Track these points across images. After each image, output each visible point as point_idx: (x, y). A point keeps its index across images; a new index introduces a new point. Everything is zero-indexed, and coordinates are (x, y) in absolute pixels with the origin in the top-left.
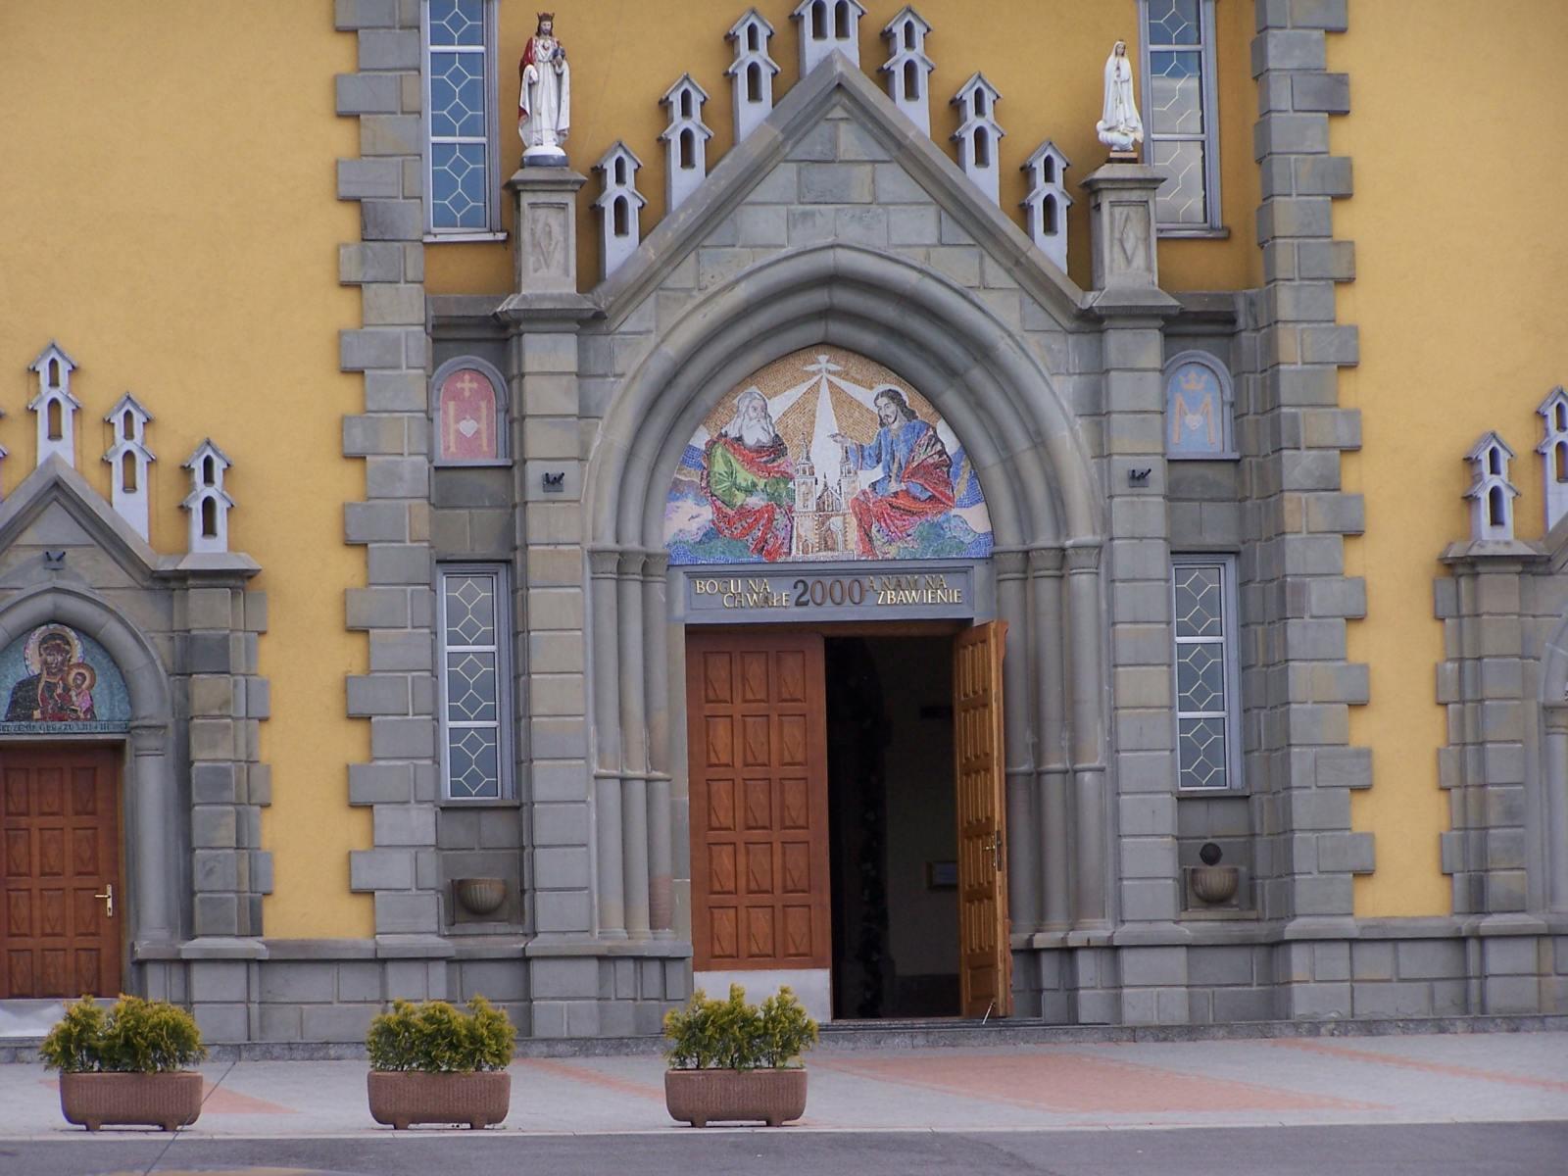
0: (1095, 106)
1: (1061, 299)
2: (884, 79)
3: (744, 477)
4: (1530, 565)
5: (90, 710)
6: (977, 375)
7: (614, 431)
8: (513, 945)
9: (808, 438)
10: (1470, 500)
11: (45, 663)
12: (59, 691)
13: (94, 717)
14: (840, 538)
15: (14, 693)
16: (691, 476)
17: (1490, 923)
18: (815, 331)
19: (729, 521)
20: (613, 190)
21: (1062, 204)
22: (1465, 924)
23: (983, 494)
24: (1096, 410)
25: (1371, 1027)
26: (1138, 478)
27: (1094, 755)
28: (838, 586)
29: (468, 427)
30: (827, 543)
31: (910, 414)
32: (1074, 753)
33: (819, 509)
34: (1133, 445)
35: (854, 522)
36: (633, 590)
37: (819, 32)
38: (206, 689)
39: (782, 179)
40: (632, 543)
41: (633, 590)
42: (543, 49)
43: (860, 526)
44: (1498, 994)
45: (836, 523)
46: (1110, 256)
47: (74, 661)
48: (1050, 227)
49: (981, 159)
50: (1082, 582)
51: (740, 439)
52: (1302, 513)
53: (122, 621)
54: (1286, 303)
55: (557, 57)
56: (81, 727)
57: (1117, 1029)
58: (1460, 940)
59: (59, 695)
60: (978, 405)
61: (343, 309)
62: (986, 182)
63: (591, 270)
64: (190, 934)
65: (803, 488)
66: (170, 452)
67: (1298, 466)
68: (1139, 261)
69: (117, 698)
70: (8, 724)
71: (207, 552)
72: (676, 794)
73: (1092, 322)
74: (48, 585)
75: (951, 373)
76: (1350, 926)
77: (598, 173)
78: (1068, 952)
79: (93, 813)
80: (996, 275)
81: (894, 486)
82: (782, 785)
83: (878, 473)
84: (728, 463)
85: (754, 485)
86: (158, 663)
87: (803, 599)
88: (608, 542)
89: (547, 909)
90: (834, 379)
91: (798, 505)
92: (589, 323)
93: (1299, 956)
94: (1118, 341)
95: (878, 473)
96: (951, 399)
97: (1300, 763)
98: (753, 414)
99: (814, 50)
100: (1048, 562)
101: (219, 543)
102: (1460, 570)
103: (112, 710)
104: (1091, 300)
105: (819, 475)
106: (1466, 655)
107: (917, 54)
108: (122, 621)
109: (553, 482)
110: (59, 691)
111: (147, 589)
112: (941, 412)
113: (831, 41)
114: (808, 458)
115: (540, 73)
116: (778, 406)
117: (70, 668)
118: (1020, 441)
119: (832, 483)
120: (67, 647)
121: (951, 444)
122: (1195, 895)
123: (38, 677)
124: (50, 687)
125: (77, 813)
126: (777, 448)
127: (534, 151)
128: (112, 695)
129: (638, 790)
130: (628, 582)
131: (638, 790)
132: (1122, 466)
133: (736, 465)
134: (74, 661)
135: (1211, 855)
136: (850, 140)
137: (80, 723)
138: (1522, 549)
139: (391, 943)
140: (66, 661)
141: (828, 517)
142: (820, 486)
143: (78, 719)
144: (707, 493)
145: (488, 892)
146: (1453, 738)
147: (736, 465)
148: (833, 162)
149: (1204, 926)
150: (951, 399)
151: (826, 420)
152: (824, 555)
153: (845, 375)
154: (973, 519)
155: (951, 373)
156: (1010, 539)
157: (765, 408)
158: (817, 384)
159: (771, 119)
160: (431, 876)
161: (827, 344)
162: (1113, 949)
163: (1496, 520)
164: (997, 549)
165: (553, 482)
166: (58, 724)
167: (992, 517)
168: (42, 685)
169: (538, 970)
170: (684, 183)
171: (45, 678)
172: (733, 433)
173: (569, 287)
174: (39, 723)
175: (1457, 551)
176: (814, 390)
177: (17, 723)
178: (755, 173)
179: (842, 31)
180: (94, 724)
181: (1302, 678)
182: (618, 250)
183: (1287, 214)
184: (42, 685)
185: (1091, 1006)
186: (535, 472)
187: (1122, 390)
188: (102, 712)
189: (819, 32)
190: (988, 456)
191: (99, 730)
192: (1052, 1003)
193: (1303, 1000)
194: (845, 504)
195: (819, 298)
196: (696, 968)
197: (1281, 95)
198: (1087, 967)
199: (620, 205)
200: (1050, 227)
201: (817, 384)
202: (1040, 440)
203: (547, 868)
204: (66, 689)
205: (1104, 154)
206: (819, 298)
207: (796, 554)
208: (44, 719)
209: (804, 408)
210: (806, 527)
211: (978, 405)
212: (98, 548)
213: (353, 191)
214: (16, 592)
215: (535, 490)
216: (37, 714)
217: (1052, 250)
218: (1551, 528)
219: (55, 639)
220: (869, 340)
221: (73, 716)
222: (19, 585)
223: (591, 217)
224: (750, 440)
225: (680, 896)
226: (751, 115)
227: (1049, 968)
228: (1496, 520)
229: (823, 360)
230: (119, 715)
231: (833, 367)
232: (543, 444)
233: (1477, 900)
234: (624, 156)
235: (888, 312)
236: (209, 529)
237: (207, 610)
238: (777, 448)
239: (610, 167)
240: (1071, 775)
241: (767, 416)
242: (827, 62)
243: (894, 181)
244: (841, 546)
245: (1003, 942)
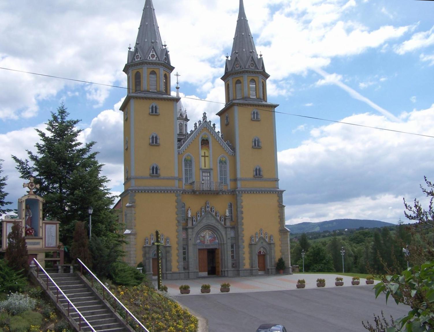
0: (226, 213)
1: (224, 226)
2: (212, 211)
3: (202, 238)
4: (255, 244)
7: (194, 236)
8: (188, 271)
9: (206, 235)
10: (251, 240)
16: (198, 238)
17: (253, 269)
18: (207, 229)
19: (201, 241)
20: (194, 219)
21: (223, 220)
22: (251, 269)
23: (218, 239)
24: (226, 234)
25: (246, 276)
26: (229, 239)
27: (226, 258)
29: (184, 235)
30: (207, 243)
31: (213, 234)
32: (224, 257)
34: (229, 236)
36: (195, 247)
37: (207, 208)
38: (168, 254)
39: (205, 218)
40: (195, 243)
41: (195, 247)
42: (189, 209)
44: (254, 274)
45: (208, 241)
46: (227, 223)
48: (223, 221)
49: (214, 212)
50: (225, 246)
52: (240, 241)
54: (239, 226)
55: (190, 210)
57: (228, 276)
58: (251, 270)
60: (218, 233)
61: (177, 228)
62: (218, 218)
63: (193, 224)
64: (167, 271)
66: (165, 238)
67: (240, 238)
68: (229, 223)
71: (168, 245)
72: (198, 261)
73: (226, 228)
75: (216, 231)
76: (244, 269)
77: (193, 218)
78: (224, 271)
80: (219, 225)
81: (212, 239)
83: (211, 238)
88: (194, 243)
89: (190, 269)
92: (192, 228)
93: (240, 271)
94: (227, 229)
95: (211, 238)
96: (216, 233)
97: (240, 258)
99: (207, 209)
101: (169, 244)
104: (225, 226)
106: (203, 158)
107: (214, 209)
109: (190, 239)
112: (215, 234)
113: (208, 209)
115: (189, 211)
116: (204, 233)
118: (221, 236)
121: (216, 236)
122: (233, 267)
127: (189, 216)
129: (196, 260)
131: (196, 260)
132: (228, 238)
135: (233, 264)
136: (210, 215)
138: (255, 243)
139: (181, 272)
144: (200, 240)
145: (186, 268)
149: (233, 269)
150: (216, 233)
151: (207, 234)
154: (217, 241)
155: (216, 231)
156: (220, 242)
158: (208, 232)
159: (205, 214)
160: (183, 267)
161: (207, 229)
162: (227, 271)
163: (253, 241)
165: (190, 239)
167: (218, 241)
169: (229, 272)
170: (198, 218)
173: (191, 226)
175: (250, 243)
176: (206, 232)
178: (204, 218)
179: (209, 208)
181: (240, 252)
182: (194, 223)
183: (239, 220)
185: (226, 275)
186: (189, 239)
187: (228, 233)
189: (207, 208)
190: (218, 237)
192: (223, 275)
193: (241, 274)
195: (207, 226)
196: (153, 275)
197: (239, 212)
198: (226, 272)
199: (194, 220)
200: (223, 221)
202: (222, 236)
203: (190, 266)
205: (226, 216)
206: (207, 226)
209: (206, 234)
210: (206, 242)
211: (218, 233)
215: (189, 240)
217: (223, 223)
220: (210, 229)
223: (192, 221)
225: (198, 268)
226: (203, 214)
227: (223, 272)
228: (253, 241)
229: (207, 230)
230: (132, 242)
232: (190, 237)
233: (252, 267)
235: (212, 227)
236: (168, 243)
237: (168, 249)
238: (204, 236)
239: (194, 217)
240: (224, 259)
242: (208, 210)
243: (213, 218)
245: (220, 270)
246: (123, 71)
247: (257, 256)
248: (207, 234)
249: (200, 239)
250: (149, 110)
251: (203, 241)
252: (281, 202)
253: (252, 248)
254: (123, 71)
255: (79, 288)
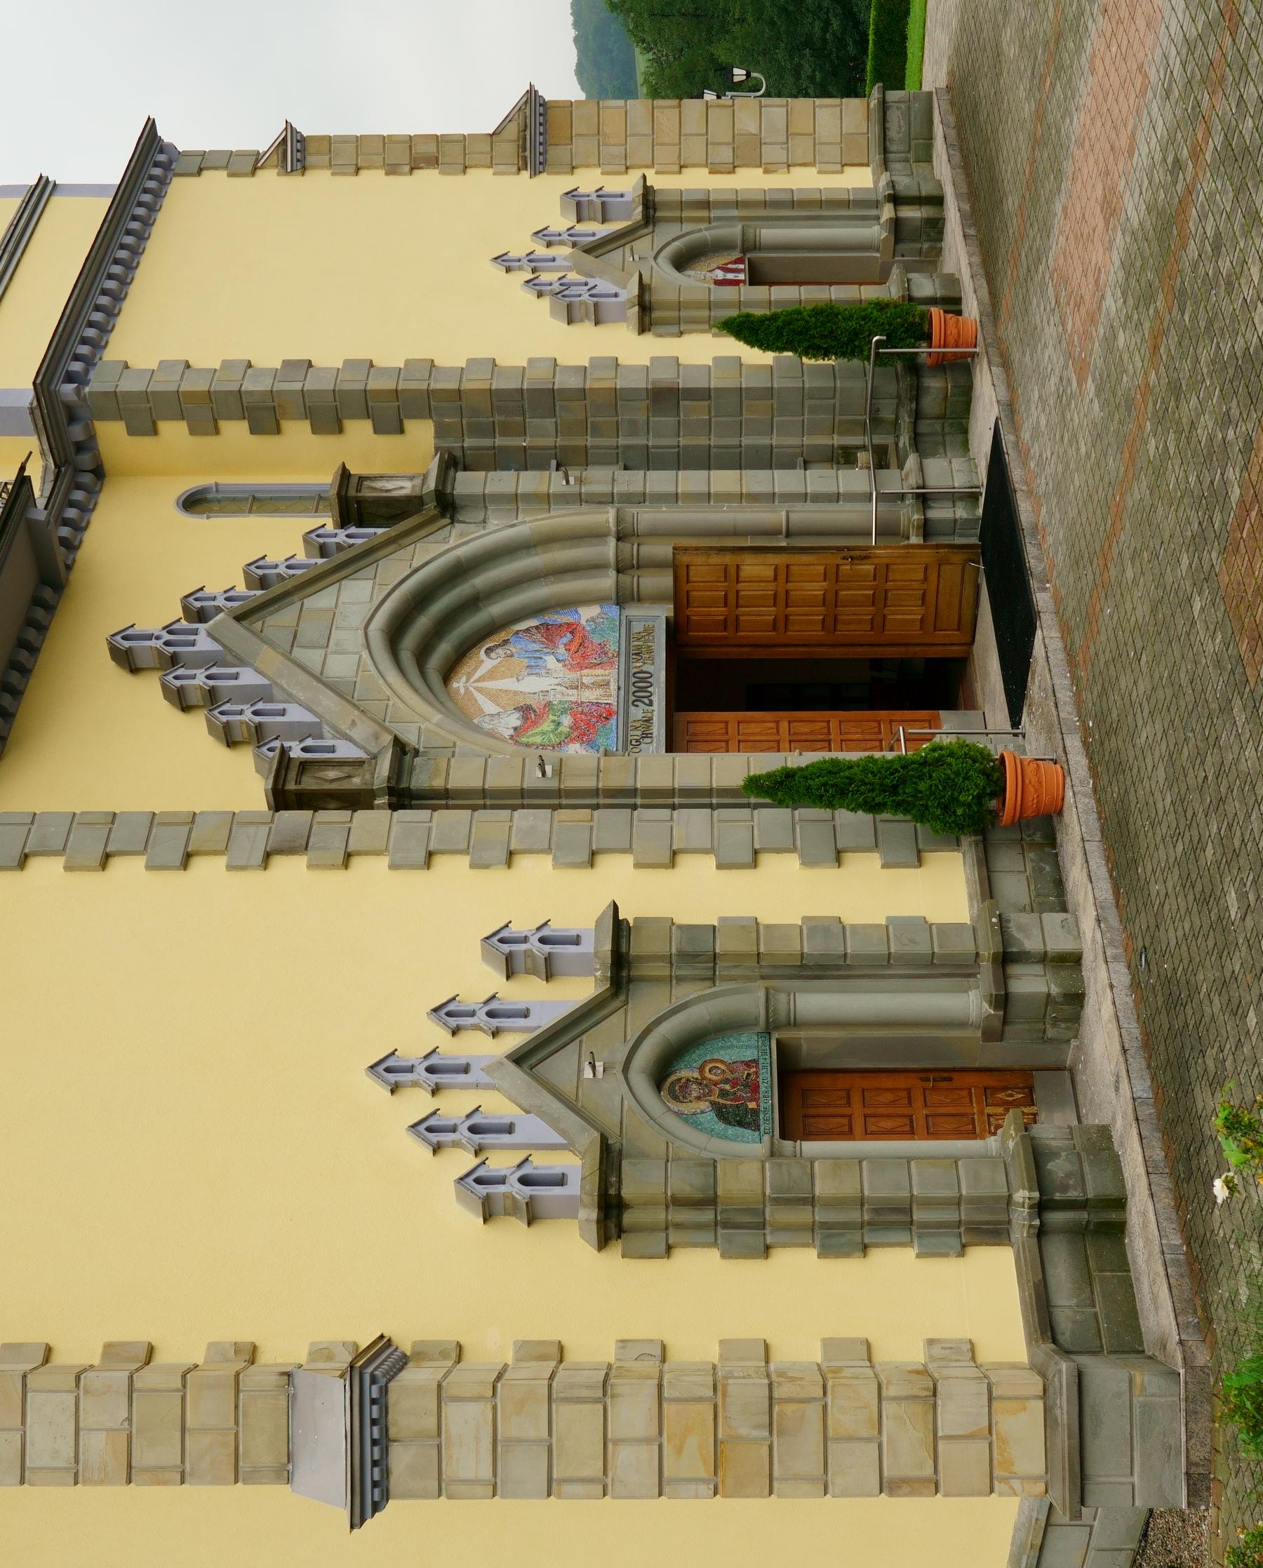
3: (547, 726)
5: (748, 1064)
6: (481, 581)
11: (699, 1098)
12: (728, 1087)
13: (755, 1061)
14: (601, 678)
15: (730, 1124)
28: (636, 694)
33: (577, 688)
35: (585, 672)
43: (591, 668)
47: (696, 1075)
51: (515, 729)
53: (658, 1022)
56: (764, 1071)
59: (733, 1087)
65: (559, 696)
69: (735, 1042)
70: (762, 1128)
74: (621, 1077)
79: (848, 1091)
81: (561, 650)
82: (795, 734)
84: (533, 735)
85: (554, 721)
86: (701, 993)
87: (647, 702)
90: (472, 680)
91: (573, 699)
98: (496, 721)
100: (627, 548)
102: (647, 320)
103: (748, 1047)
105: (549, 688)
108: (658, 1022)
110: (728, 1087)
111: (626, 1003)
114: (535, 693)
116: (489, 707)
117: (704, 1078)
119: (557, 681)
120: (683, 1081)
123: (713, 1103)
124: (724, 1094)
125: (849, 1104)
126: (526, 710)
128: (732, 1047)
130: (641, 589)
133: (536, 731)
134: (696, 1075)
137: (761, 1072)
140: (697, 1082)
141: (583, 683)
142: (558, 688)
143: (756, 1073)
146: (709, 1236)
147: (536, 731)
148: (296, 631)
151: (509, 684)
152: (613, 686)
153: (469, 676)
155: (473, 602)
157: (491, 715)
158: (478, 680)
164: (614, 597)
166: (762, 1089)
168: (721, 1101)
171: (715, 1098)
172: (511, 732)
174: (762, 1105)
177: (761, 1122)
180: (761, 1061)
184: (721, 1101)
188: (749, 1055)
191: (768, 1057)
194: (574, 676)
201: (475, 688)
204: (726, 1081)
207: (613, 700)
208: (757, 1100)
209: (493, 696)
212: (584, 1037)
213: (260, 855)
214: (626, 1102)
216: (752, 1105)
218: (565, 1142)
219: (675, 1091)
221: (753, 1077)
222: (618, 1099)
224: (518, 723)
230: (753, 1042)
231: (464, 679)
234: (268, 747)
238: (526, 710)
241: (498, 714)
244: (607, 678)
246: (721, 1342)
247: (811, 1147)
248: (509, 684)
249: (554, 740)
250: (1010, 408)
251: (574, 715)
252: (257, 161)
253: (679, 306)
254: (721, 1342)
255: (949, 1228)
